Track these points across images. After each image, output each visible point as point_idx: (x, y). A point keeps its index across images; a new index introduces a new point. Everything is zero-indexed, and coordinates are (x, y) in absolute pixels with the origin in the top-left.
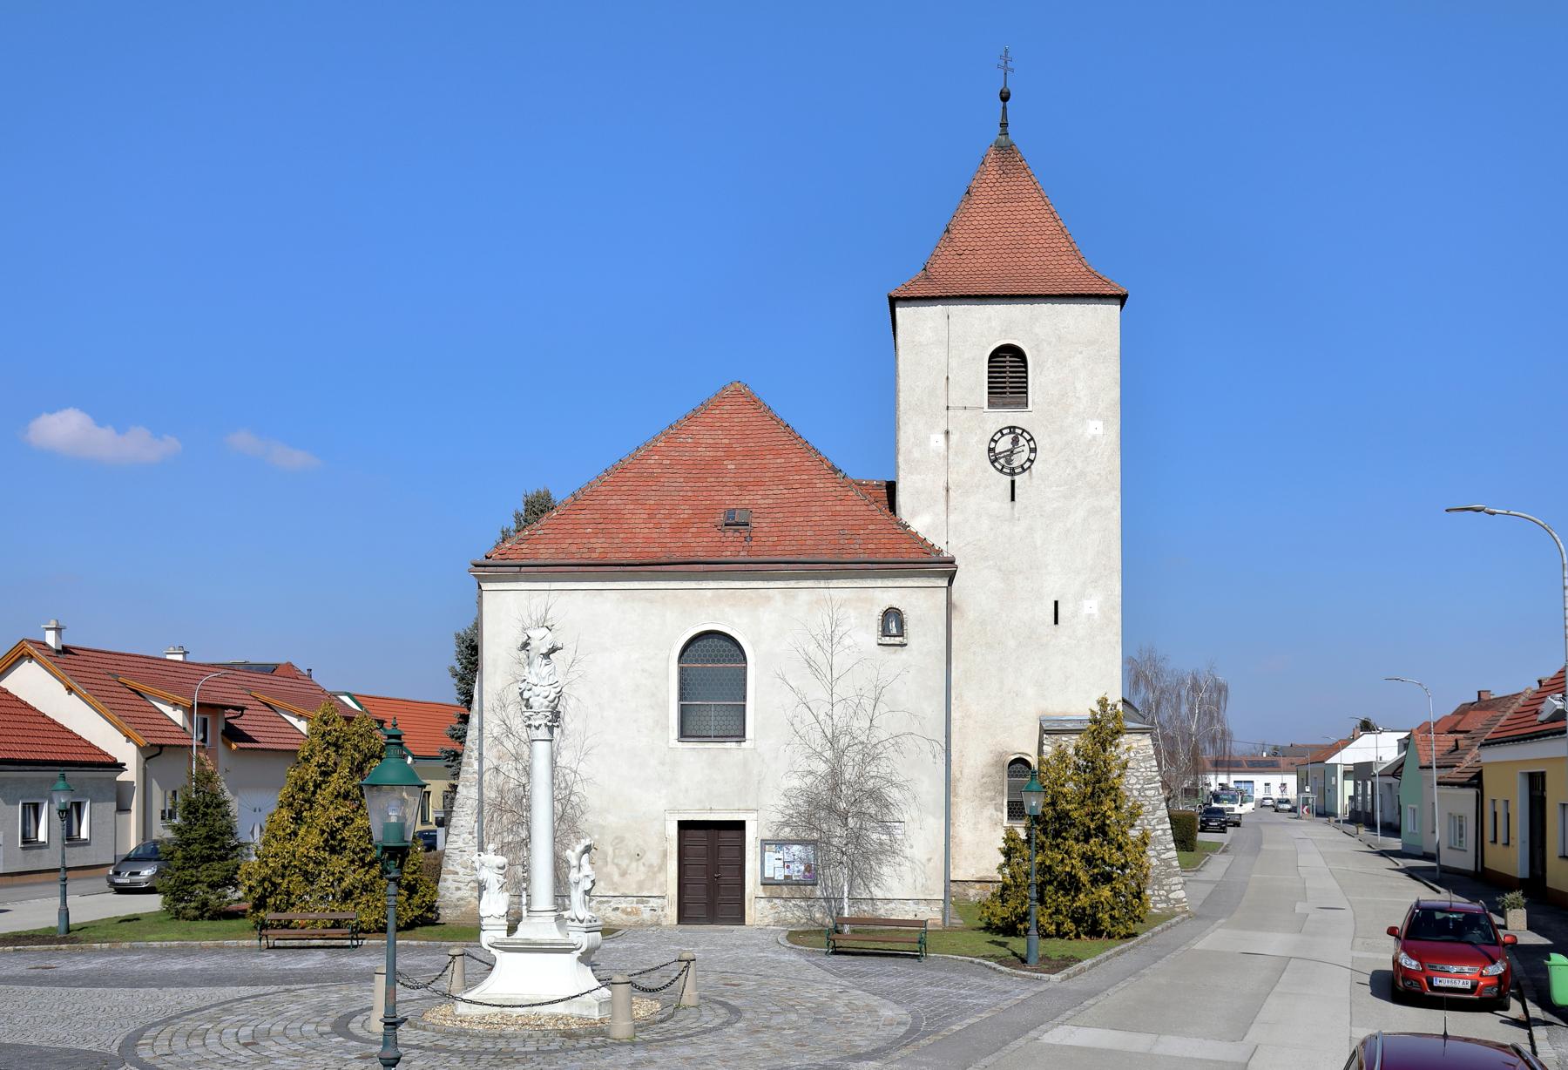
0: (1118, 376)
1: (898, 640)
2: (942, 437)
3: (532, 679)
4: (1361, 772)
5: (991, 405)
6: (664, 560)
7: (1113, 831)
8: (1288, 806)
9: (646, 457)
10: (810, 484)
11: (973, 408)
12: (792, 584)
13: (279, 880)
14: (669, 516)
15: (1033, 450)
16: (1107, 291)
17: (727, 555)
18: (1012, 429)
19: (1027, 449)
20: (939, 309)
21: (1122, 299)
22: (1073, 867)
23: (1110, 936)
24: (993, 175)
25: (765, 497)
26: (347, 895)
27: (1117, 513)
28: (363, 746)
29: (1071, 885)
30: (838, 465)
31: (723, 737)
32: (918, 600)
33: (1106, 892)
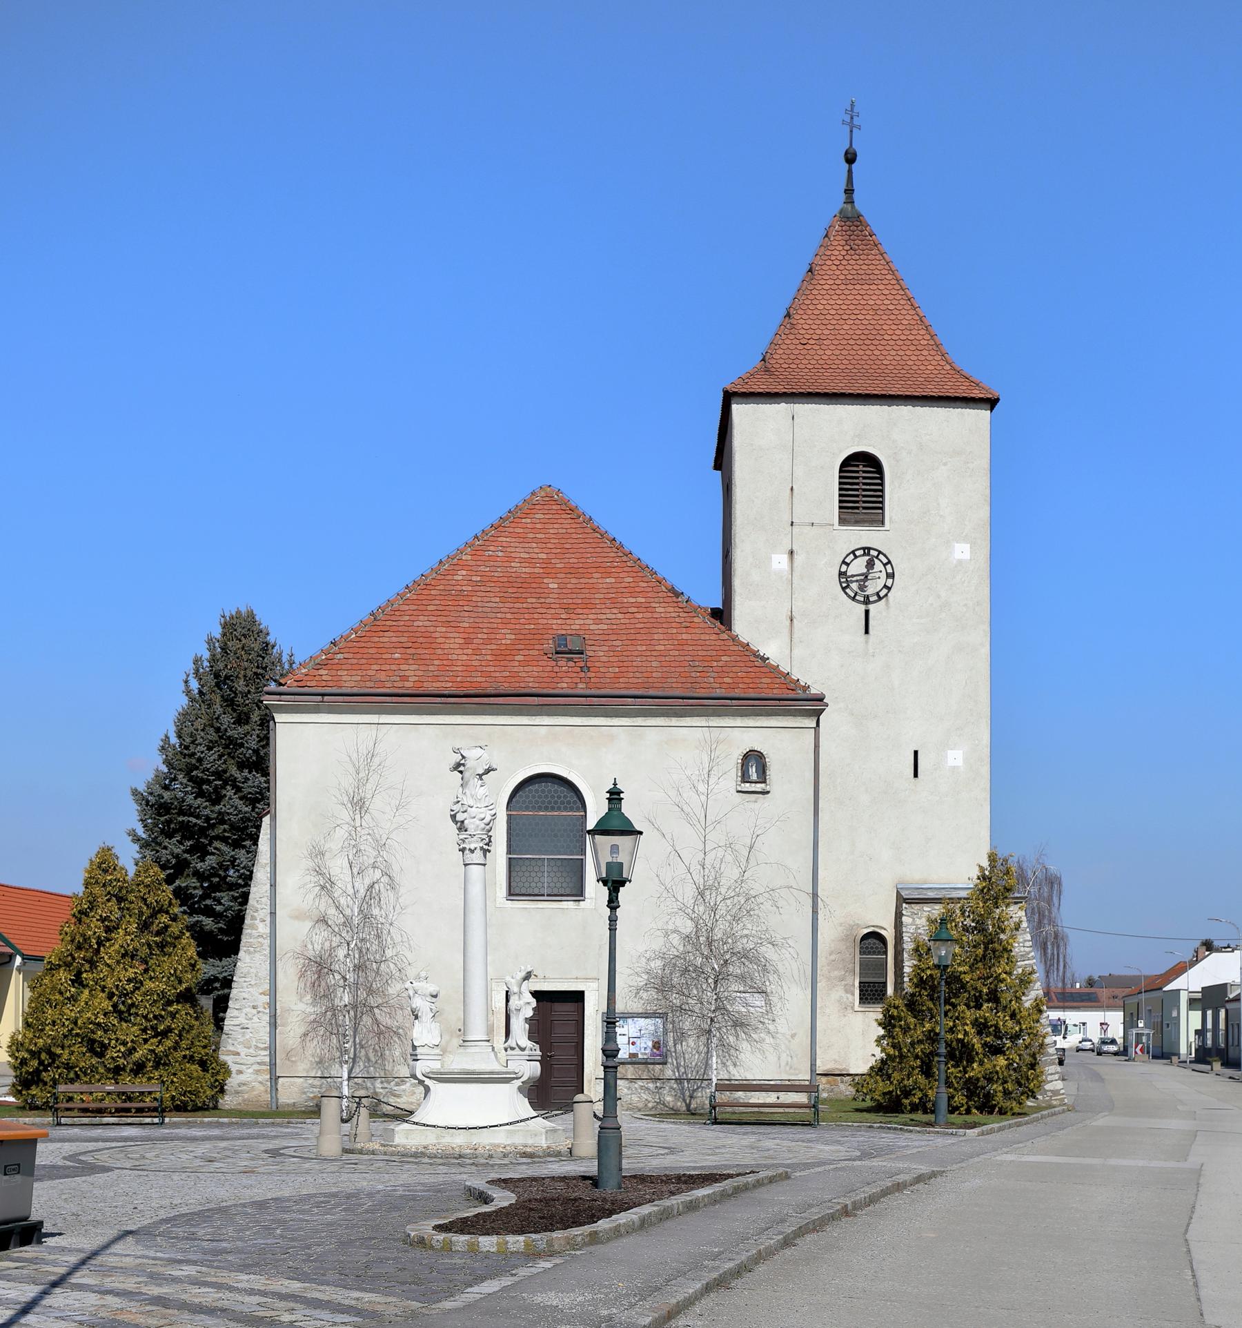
0: (988, 492)
1: (759, 787)
2: (785, 557)
3: (468, 801)
4: (1212, 998)
5: (842, 521)
6: (490, 691)
7: (1005, 998)
8: (1113, 1048)
9: (452, 572)
10: (648, 608)
11: (821, 525)
12: (639, 721)
13: (59, 1051)
14: (488, 641)
15: (891, 576)
16: (977, 394)
17: (563, 687)
18: (866, 550)
19: (883, 575)
20: (782, 408)
21: (991, 403)
22: (966, 1033)
23: (1002, 1112)
24: (838, 251)
25: (598, 622)
26: (139, 1068)
27: (985, 650)
28: (151, 899)
29: (961, 1054)
30: (679, 588)
31: (556, 895)
32: (779, 739)
33: (1001, 1061)
